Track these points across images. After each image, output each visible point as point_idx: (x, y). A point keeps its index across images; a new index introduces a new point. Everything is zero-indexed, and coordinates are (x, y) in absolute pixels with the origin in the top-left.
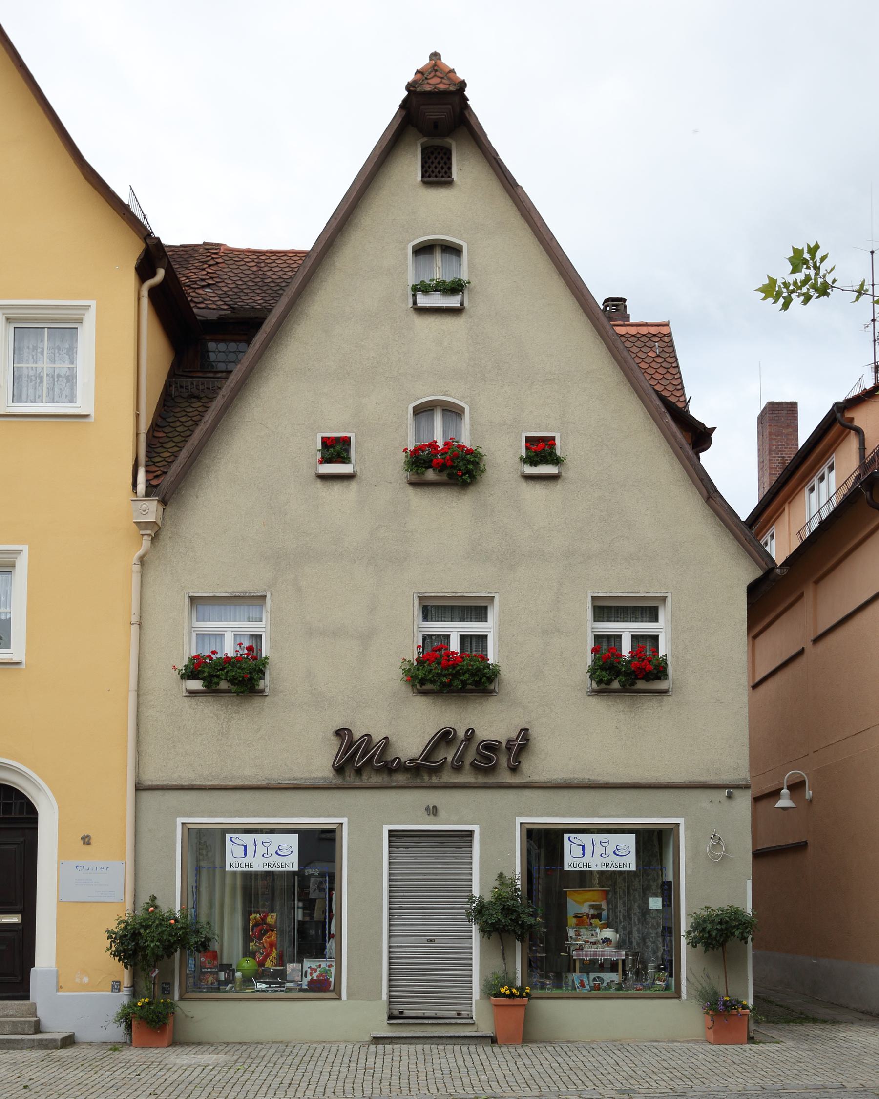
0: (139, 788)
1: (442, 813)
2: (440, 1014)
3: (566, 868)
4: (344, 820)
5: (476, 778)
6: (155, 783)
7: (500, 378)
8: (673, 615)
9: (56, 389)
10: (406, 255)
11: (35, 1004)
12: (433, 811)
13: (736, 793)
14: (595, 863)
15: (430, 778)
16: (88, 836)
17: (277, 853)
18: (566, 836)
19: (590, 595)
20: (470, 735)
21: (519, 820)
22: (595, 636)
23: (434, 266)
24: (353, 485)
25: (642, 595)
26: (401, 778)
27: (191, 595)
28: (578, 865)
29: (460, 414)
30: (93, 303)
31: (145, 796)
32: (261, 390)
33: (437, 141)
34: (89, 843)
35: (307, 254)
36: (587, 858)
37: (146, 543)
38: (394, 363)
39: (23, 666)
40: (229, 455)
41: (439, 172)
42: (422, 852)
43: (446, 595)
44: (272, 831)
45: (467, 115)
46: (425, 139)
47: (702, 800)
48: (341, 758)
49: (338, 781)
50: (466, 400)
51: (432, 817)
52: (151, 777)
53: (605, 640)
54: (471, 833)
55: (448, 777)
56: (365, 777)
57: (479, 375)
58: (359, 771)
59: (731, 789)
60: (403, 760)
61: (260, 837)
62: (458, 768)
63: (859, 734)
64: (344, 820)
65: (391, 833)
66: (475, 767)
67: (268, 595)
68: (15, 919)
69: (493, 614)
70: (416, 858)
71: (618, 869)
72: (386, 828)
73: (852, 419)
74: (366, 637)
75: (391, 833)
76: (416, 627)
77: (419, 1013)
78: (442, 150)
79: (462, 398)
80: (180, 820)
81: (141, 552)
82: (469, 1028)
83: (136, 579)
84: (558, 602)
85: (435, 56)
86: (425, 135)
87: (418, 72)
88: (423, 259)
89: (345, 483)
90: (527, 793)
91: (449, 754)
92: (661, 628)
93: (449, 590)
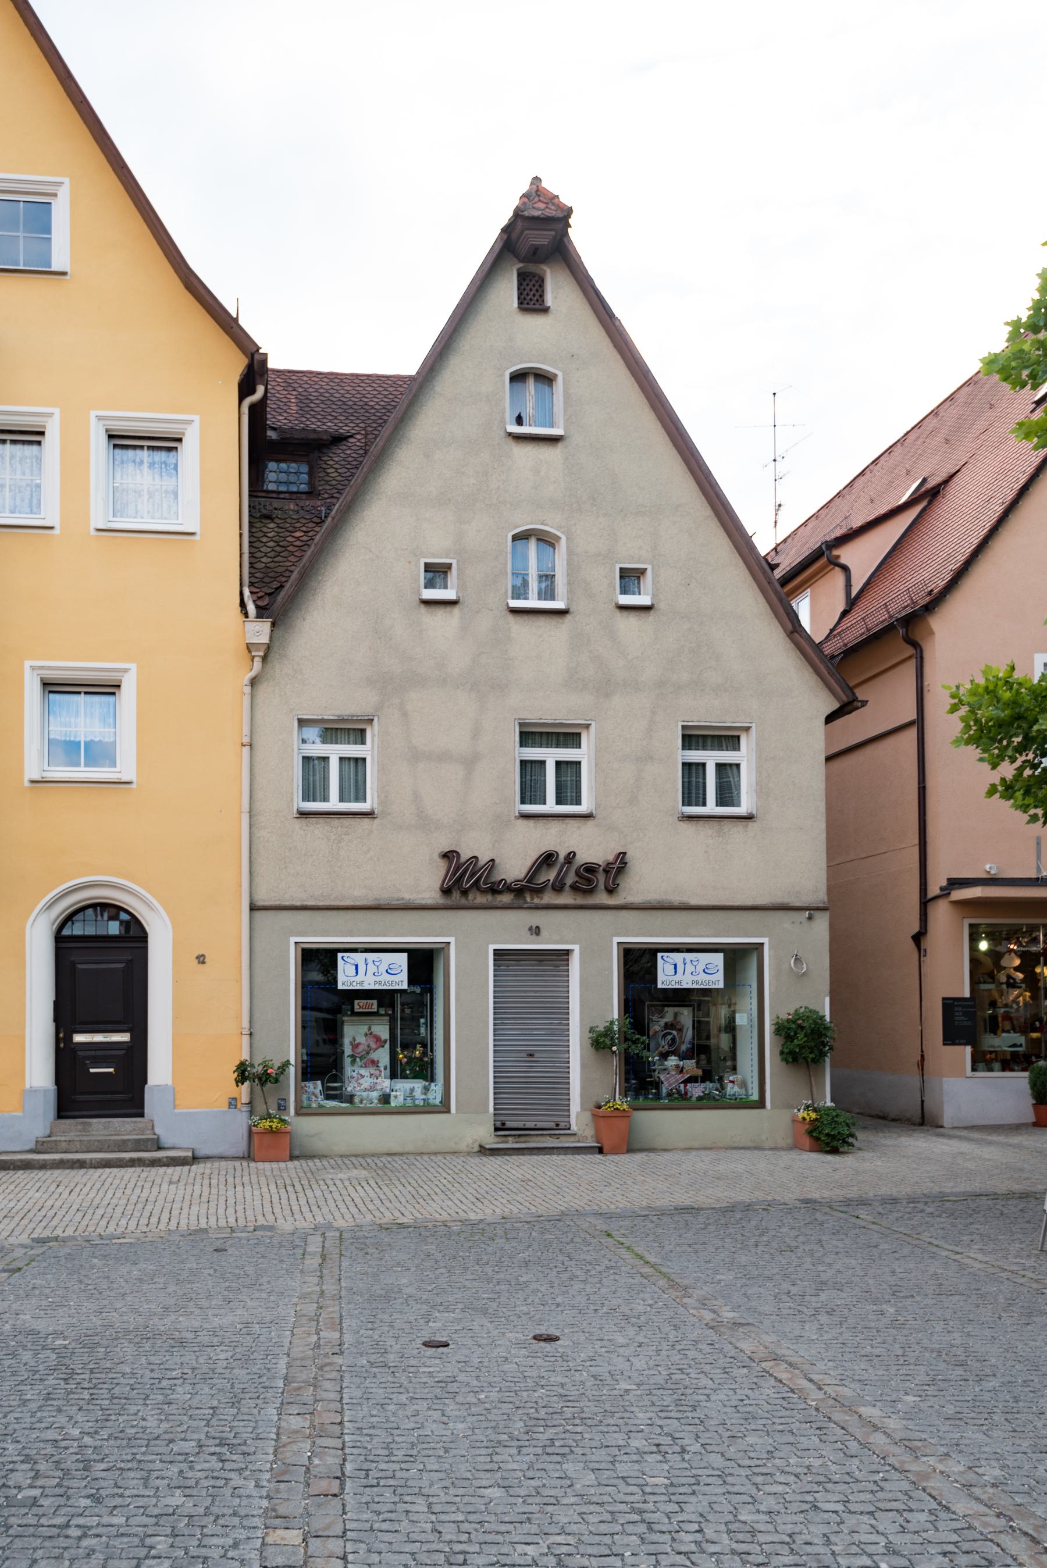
0: (253, 908)
1: (544, 932)
2: (540, 1125)
3: (660, 986)
4: (451, 939)
5: (575, 899)
6: (267, 904)
7: (595, 508)
8: (757, 744)
9: (164, 505)
10: (504, 383)
11: (152, 1121)
12: (536, 931)
13: (817, 915)
14: (368, 982)
15: (532, 899)
16: (203, 955)
17: (387, 971)
18: (340, 955)
19: (680, 724)
20: (570, 857)
21: (616, 939)
22: (304, 758)
23: (528, 394)
24: (456, 610)
25: (729, 725)
26: (506, 898)
27: (300, 717)
28: (351, 983)
29: (553, 544)
30: (196, 418)
31: (258, 915)
32: (365, 513)
33: (532, 268)
34: (203, 962)
35: (411, 378)
36: (679, 976)
37: (258, 664)
38: (494, 491)
39: (134, 786)
40: (334, 578)
41: (531, 300)
42: (522, 970)
43: (546, 721)
44: (678, 950)
45: (567, 243)
46: (521, 265)
47: (785, 920)
48: (450, 880)
49: (448, 902)
50: (563, 530)
51: (534, 936)
52: (264, 898)
53: (352, 763)
54: (568, 953)
55: (549, 898)
56: (471, 896)
57: (575, 505)
58: (465, 893)
59: (811, 910)
60: (508, 881)
61: (689, 956)
62: (558, 887)
63: (871, 858)
64: (451, 939)
65: (497, 953)
66: (574, 888)
67: (376, 719)
68: (124, 1037)
69: (586, 740)
70: (516, 976)
71: (707, 987)
72: (492, 948)
73: (838, 557)
74: (470, 762)
75: (497, 953)
76: (517, 752)
77: (520, 1125)
78: (534, 277)
79: (559, 528)
80: (293, 940)
81: (253, 674)
82: (572, 1139)
83: (247, 700)
84: (651, 730)
85: (536, 180)
86: (522, 261)
87: (524, 196)
88: (518, 385)
89: (449, 609)
90: (624, 913)
91: (551, 875)
92: (582, 754)
93: (548, 717)
